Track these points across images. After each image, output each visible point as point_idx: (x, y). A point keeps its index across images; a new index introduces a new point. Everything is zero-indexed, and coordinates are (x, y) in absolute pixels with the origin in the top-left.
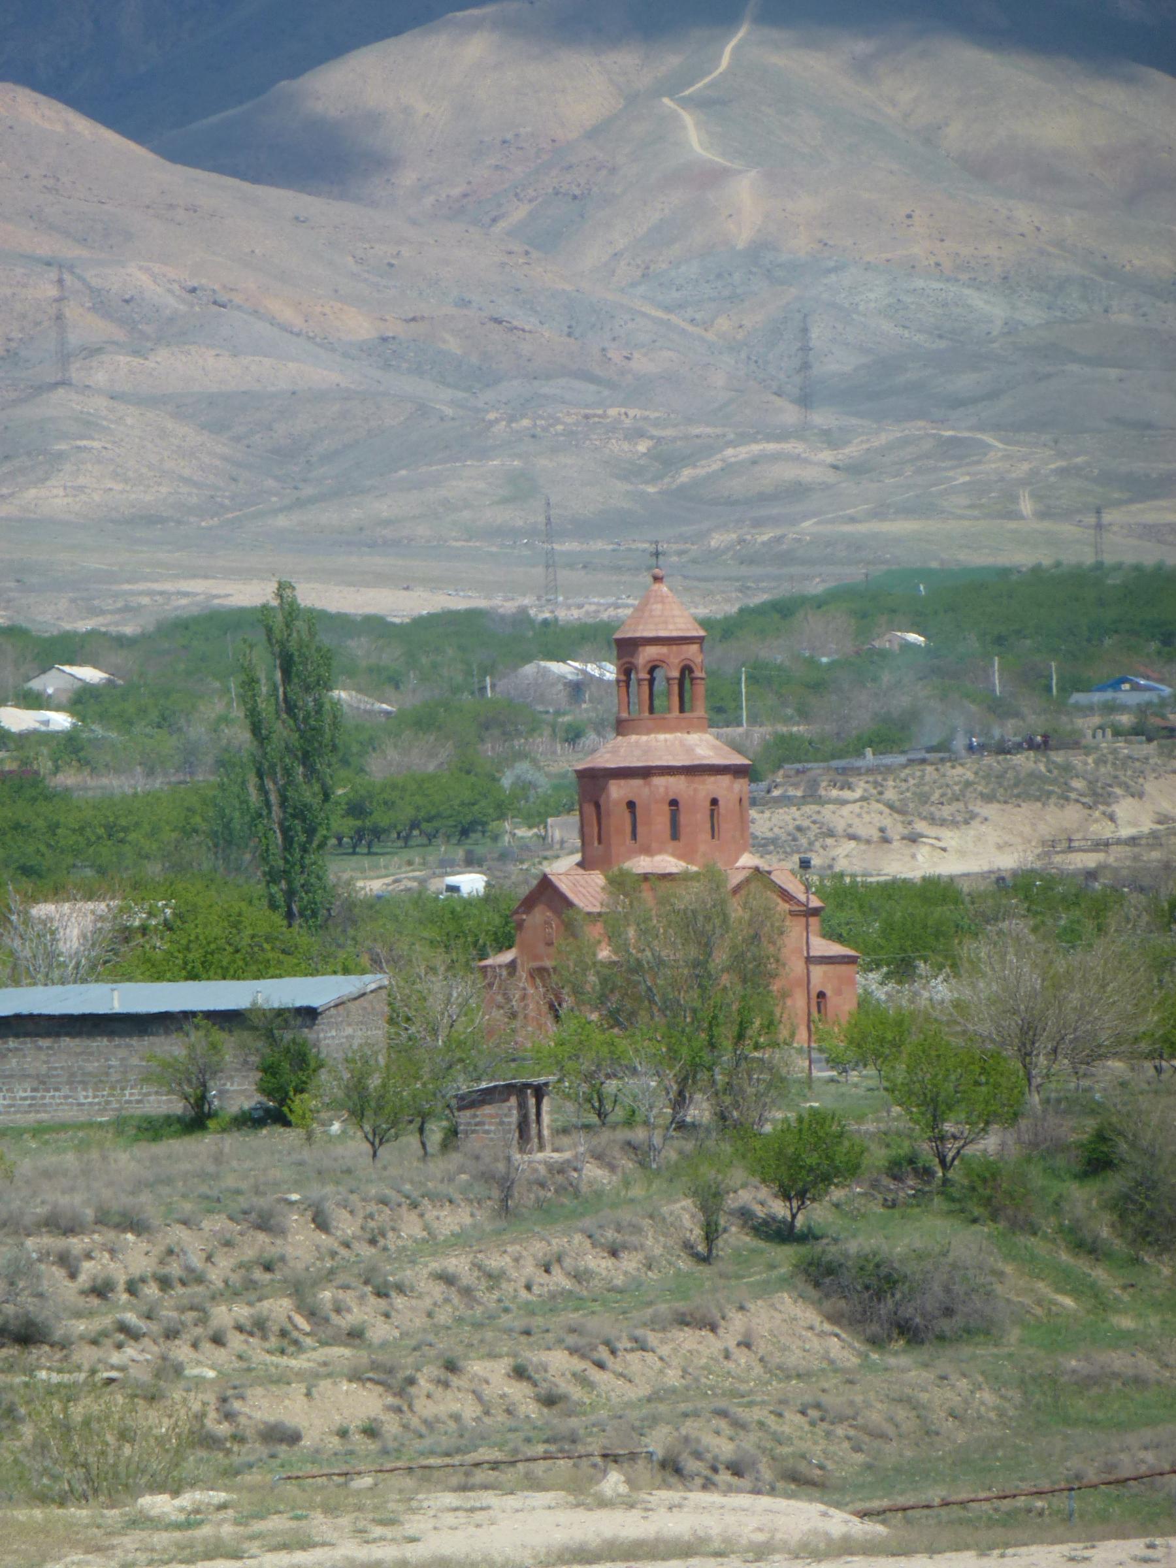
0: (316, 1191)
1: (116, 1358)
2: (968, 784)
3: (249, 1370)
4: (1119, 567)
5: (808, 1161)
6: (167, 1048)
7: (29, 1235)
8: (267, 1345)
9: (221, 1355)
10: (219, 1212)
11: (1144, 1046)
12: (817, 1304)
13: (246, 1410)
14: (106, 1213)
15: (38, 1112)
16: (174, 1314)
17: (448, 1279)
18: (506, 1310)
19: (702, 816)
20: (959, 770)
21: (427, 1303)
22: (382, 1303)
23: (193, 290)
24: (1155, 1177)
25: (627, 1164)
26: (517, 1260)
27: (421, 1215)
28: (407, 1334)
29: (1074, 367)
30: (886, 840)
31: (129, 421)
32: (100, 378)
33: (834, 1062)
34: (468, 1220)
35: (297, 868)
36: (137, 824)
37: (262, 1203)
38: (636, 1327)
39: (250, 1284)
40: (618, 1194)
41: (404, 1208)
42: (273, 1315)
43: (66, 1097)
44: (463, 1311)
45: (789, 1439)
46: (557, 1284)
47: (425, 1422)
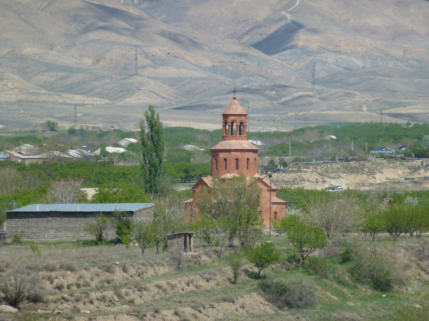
0: (124, 261)
1: (60, 307)
2: (339, 168)
3: (99, 311)
4: (386, 123)
6: (92, 221)
8: (105, 304)
9: (92, 306)
11: (361, 228)
12: (264, 296)
14: (63, 265)
15: (56, 238)
17: (159, 287)
18: (175, 296)
19: (245, 163)
20: (337, 165)
21: (153, 293)
22: (140, 293)
23: (169, 53)
24: (361, 264)
25: (214, 256)
26: (180, 282)
27: (154, 269)
28: (146, 302)
29: (378, 77)
30: (317, 182)
31: (152, 83)
32: (146, 73)
33: (278, 231)
36: (130, 173)
37: (108, 264)
39: (103, 287)
40: (211, 265)
41: (149, 267)
42: (108, 295)
43: (64, 234)
44: (163, 296)
46: (191, 289)
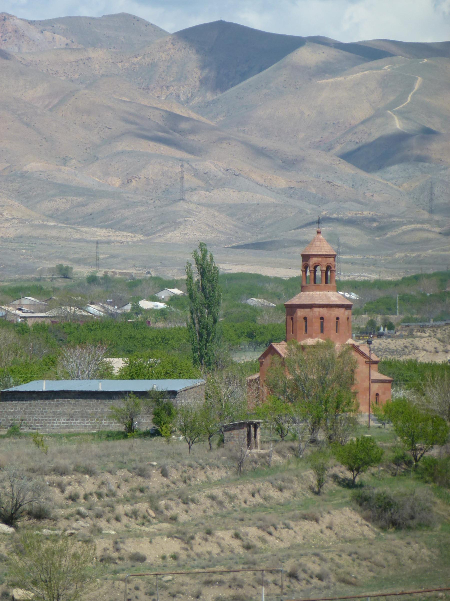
0: (163, 461)
1: (75, 525)
3: (129, 531)
5: (360, 457)
7: (46, 475)
8: (137, 522)
10: (125, 468)
12: (360, 513)
13: (124, 547)
14: (78, 467)
15: (69, 428)
16: (100, 508)
17: (213, 498)
18: (236, 511)
21: (204, 507)
22: (185, 506)
23: (227, 170)
25: (290, 455)
26: (241, 491)
27: (205, 472)
30: (437, 352)
31: (203, 212)
32: (195, 198)
34: (224, 475)
35: (204, 347)
37: (141, 465)
38: (286, 519)
39: (134, 497)
42: (141, 509)
44: (218, 510)
45: (343, 566)
46: (257, 501)
47: (197, 555)
